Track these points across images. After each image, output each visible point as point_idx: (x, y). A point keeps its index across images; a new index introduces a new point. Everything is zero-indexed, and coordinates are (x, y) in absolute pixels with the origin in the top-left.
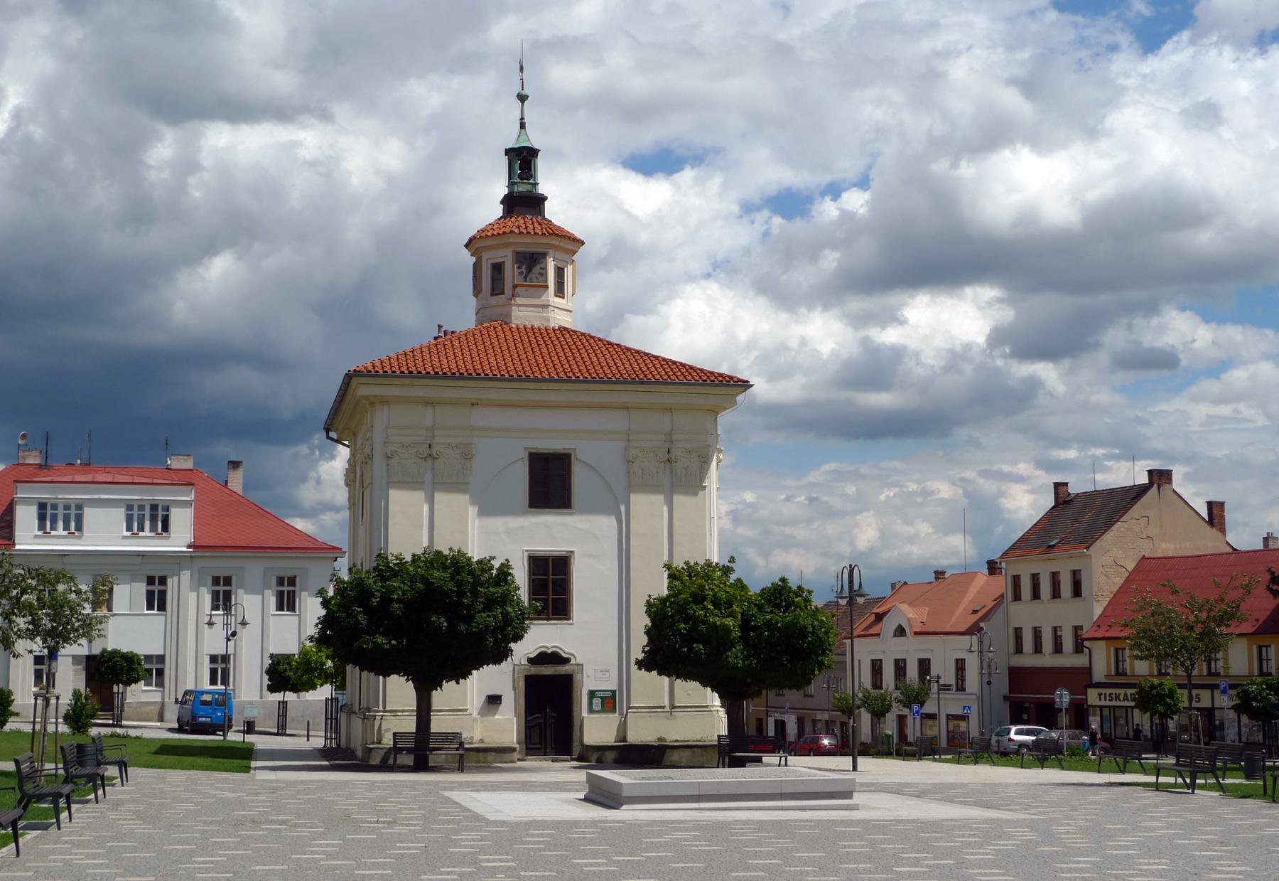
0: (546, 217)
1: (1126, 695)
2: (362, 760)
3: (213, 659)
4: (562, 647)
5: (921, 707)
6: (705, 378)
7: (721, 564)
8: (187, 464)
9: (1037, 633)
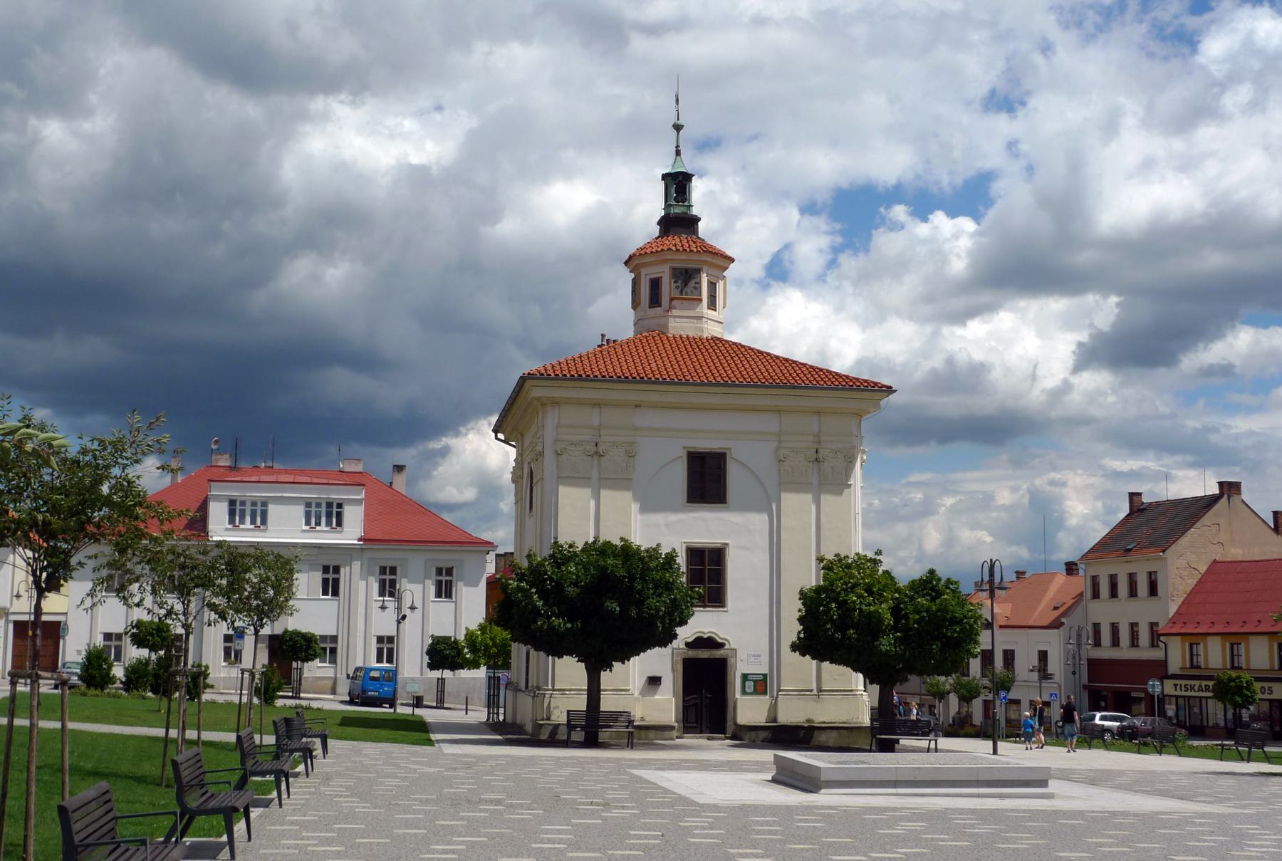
0: (699, 236)
1: (1200, 686)
3: (380, 639)
4: (717, 632)
5: (1008, 692)
6: (851, 384)
9: (1115, 629)
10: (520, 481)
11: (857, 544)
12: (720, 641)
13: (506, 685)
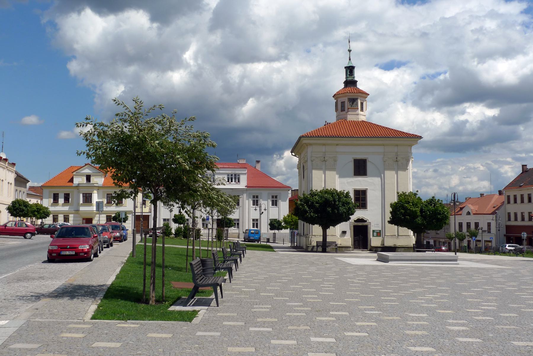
2: (306, 249)
3: (253, 220)
6: (408, 136)
7: (414, 193)
8: (244, 162)
9: (516, 214)
10: (300, 169)
11: (410, 189)
12: (365, 220)
13: (297, 234)
